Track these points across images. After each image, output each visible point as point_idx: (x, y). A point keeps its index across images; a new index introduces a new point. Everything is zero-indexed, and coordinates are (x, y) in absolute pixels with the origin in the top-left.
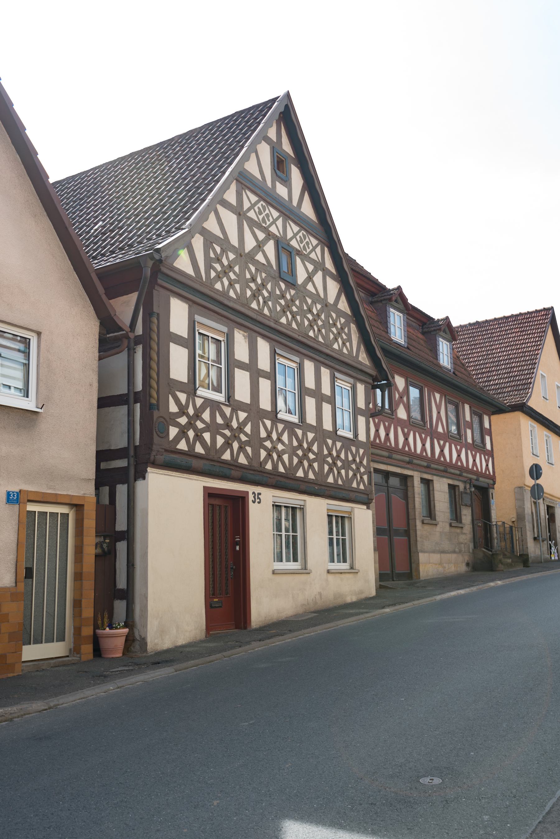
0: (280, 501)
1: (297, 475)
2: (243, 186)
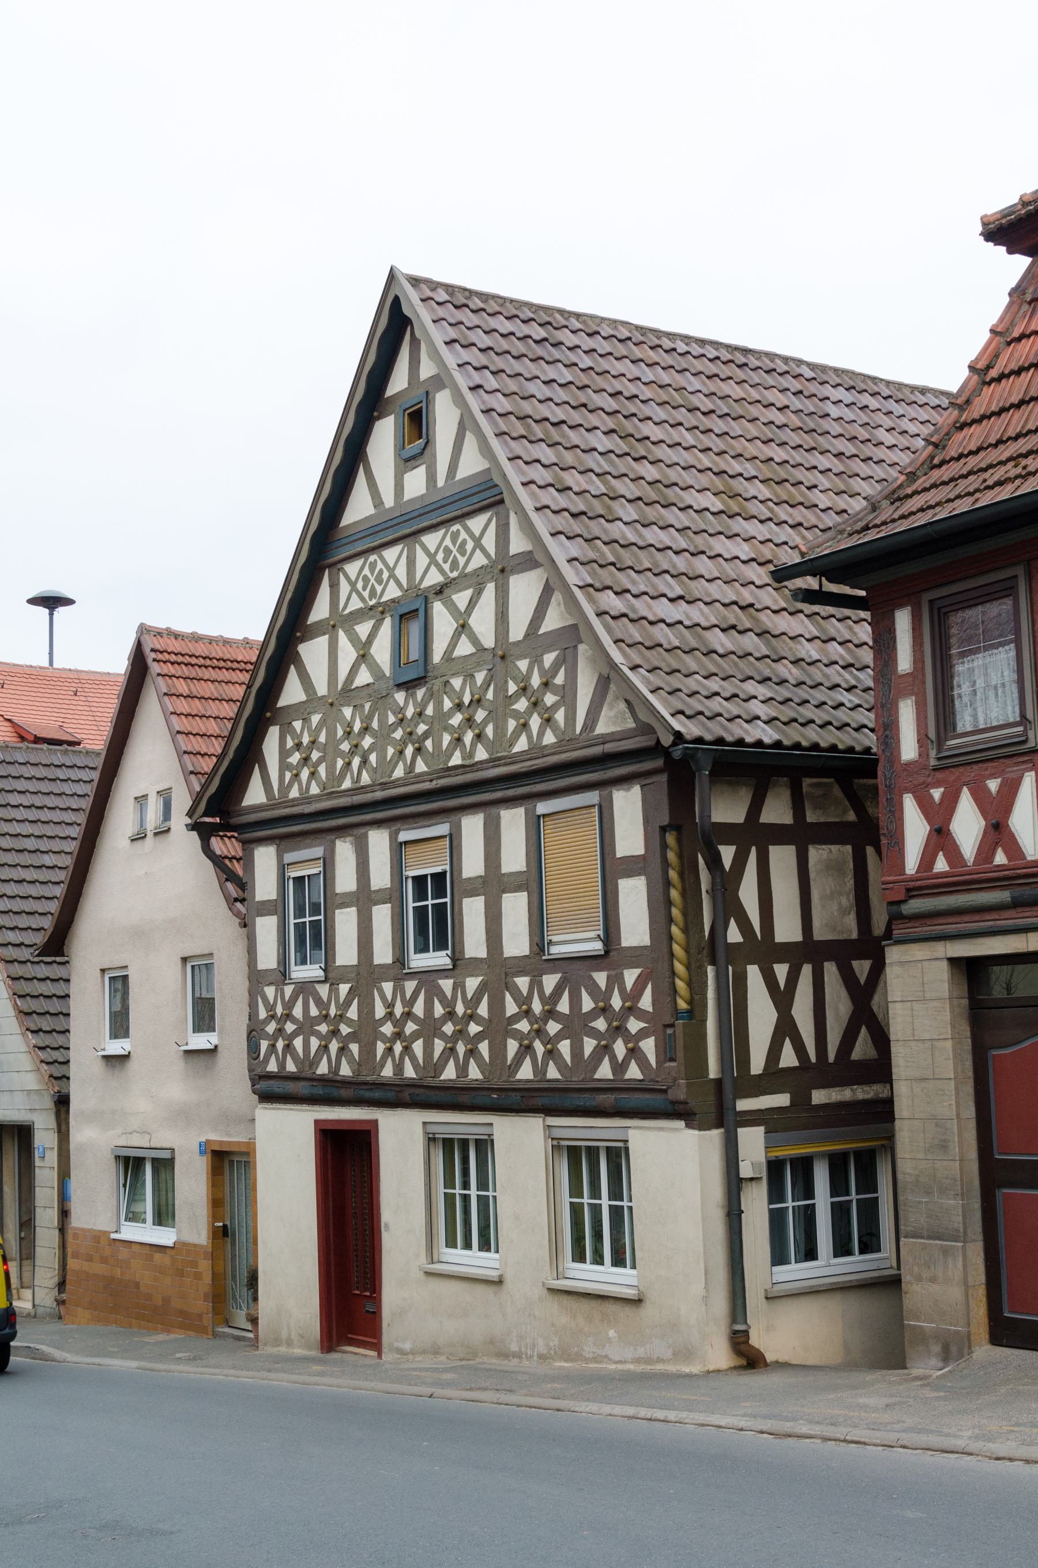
0: (443, 1132)
1: (627, 1076)
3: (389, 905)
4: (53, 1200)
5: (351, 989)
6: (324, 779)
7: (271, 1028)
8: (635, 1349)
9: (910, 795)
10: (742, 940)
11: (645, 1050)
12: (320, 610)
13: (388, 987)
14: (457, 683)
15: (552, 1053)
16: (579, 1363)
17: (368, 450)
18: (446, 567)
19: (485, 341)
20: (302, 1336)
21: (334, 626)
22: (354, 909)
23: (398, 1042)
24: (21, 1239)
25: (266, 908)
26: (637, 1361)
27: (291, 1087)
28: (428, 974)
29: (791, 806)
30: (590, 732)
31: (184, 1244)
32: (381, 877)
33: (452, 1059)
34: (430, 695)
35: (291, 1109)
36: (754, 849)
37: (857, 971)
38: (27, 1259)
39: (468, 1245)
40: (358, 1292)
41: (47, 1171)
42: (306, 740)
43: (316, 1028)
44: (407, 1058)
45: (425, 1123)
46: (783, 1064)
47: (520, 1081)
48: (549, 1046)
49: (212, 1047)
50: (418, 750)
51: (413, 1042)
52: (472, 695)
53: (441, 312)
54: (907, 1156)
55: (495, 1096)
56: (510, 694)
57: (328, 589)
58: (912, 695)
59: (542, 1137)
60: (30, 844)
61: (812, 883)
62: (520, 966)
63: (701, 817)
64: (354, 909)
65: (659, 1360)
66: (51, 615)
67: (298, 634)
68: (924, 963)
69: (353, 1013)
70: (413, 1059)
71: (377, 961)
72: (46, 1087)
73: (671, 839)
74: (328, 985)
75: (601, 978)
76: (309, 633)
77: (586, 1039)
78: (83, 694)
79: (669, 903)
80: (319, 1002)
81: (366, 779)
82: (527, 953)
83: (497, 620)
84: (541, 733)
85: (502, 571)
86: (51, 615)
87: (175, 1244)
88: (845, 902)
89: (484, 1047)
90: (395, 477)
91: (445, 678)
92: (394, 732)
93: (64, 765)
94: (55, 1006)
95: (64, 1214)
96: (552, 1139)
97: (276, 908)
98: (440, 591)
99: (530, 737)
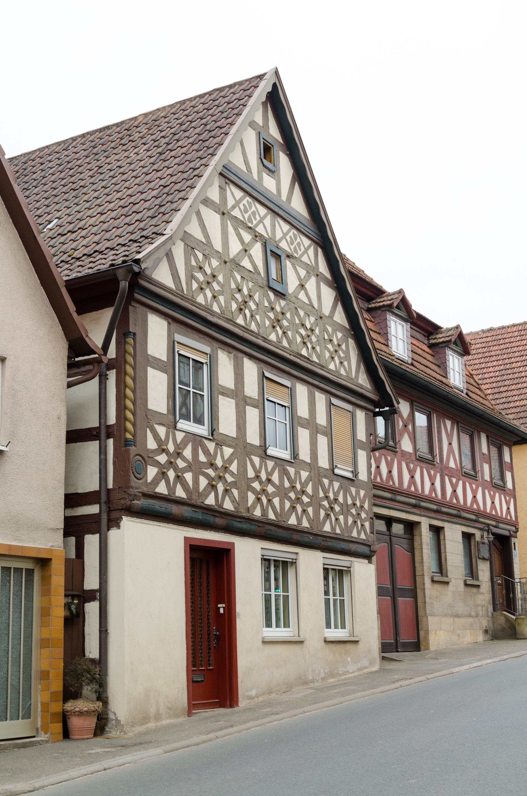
0: (272, 555)
2: (227, 181)
8: (357, 665)
16: (338, 677)
26: (358, 670)
27: (175, 509)
55: (311, 538)
65: (365, 668)
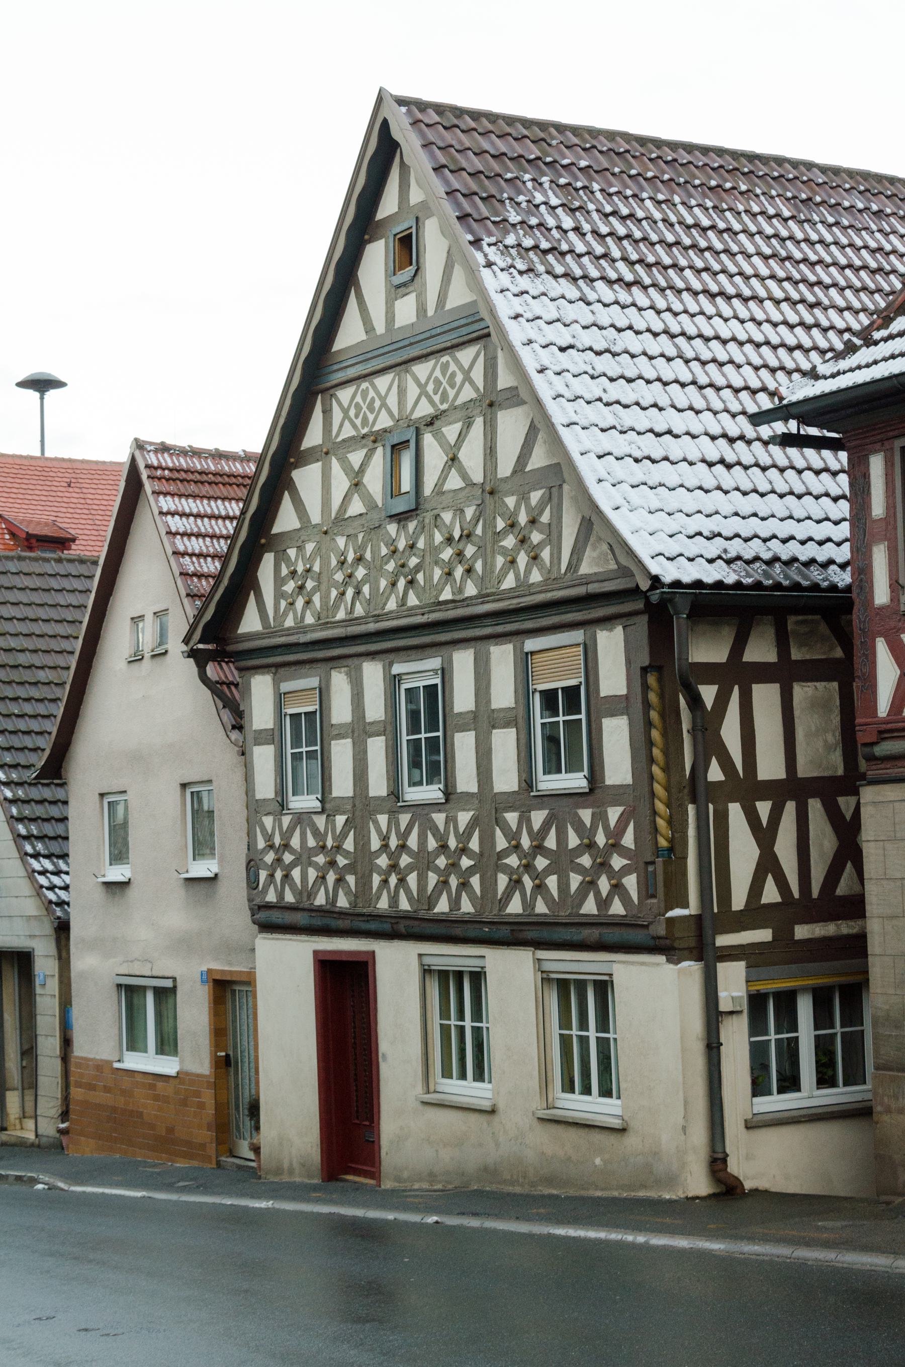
0: (438, 963)
1: (611, 912)
3: (383, 738)
4: (55, 1029)
5: (347, 820)
6: (319, 609)
7: (270, 858)
9: (882, 639)
10: (723, 778)
11: (628, 887)
12: (313, 437)
13: (383, 819)
14: (447, 517)
15: (540, 887)
17: (359, 273)
18: (437, 398)
19: (477, 164)
20: (303, 1165)
21: (327, 453)
22: (349, 741)
23: (393, 875)
24: (23, 1068)
25: (263, 738)
28: (421, 807)
29: (775, 644)
30: (574, 572)
31: (187, 1074)
32: (375, 710)
33: (445, 892)
34: (422, 528)
35: (290, 940)
36: (736, 688)
37: (843, 807)
38: (29, 1088)
39: (463, 1076)
40: (358, 1122)
41: (48, 999)
42: (300, 569)
43: (314, 859)
44: (402, 891)
45: (420, 956)
46: (765, 900)
47: (510, 915)
48: (537, 882)
49: (212, 875)
50: (411, 582)
51: (408, 875)
52: (462, 531)
53: (431, 135)
54: (878, 991)
56: (498, 530)
57: (321, 414)
58: (886, 539)
59: (532, 969)
60: (22, 659)
61: (796, 721)
62: (508, 801)
63: (679, 659)
64: (349, 741)
66: (42, 398)
67: (292, 460)
68: (895, 804)
69: (349, 845)
70: (408, 892)
71: (372, 793)
72: (46, 913)
73: (652, 680)
74: (324, 816)
75: (586, 815)
76: (305, 459)
77: (572, 875)
78: (78, 485)
79: (650, 743)
80: (316, 833)
81: (359, 610)
82: (516, 788)
83: (485, 455)
84: (528, 571)
85: (491, 405)
86: (42, 398)
87: (178, 1073)
88: (830, 738)
89: (475, 881)
90: (386, 303)
91: (435, 512)
92: (386, 564)
93: (58, 574)
94: (54, 811)
95: (67, 1042)
96: (542, 972)
97: (271, 737)
98: (431, 422)
99: (517, 576)
